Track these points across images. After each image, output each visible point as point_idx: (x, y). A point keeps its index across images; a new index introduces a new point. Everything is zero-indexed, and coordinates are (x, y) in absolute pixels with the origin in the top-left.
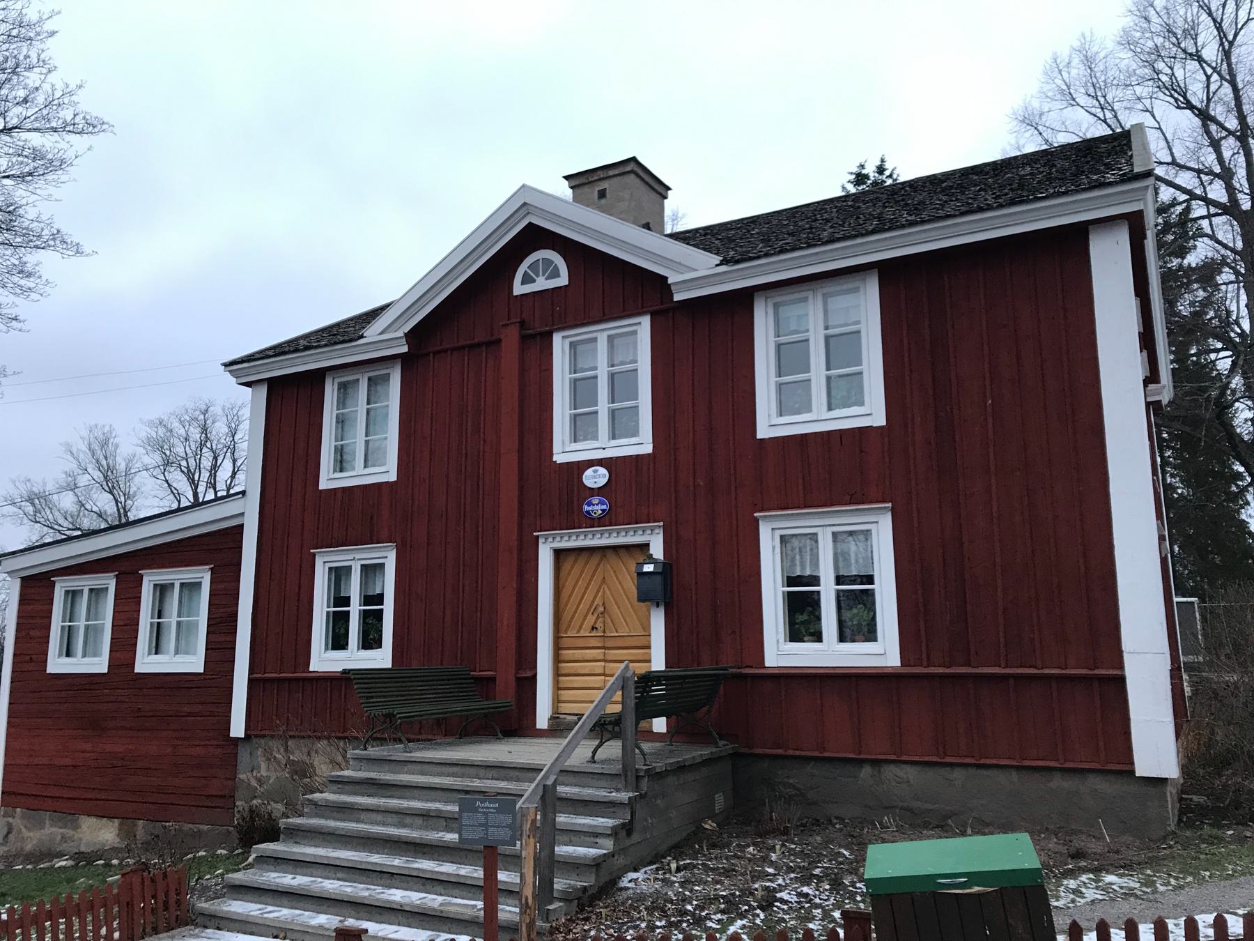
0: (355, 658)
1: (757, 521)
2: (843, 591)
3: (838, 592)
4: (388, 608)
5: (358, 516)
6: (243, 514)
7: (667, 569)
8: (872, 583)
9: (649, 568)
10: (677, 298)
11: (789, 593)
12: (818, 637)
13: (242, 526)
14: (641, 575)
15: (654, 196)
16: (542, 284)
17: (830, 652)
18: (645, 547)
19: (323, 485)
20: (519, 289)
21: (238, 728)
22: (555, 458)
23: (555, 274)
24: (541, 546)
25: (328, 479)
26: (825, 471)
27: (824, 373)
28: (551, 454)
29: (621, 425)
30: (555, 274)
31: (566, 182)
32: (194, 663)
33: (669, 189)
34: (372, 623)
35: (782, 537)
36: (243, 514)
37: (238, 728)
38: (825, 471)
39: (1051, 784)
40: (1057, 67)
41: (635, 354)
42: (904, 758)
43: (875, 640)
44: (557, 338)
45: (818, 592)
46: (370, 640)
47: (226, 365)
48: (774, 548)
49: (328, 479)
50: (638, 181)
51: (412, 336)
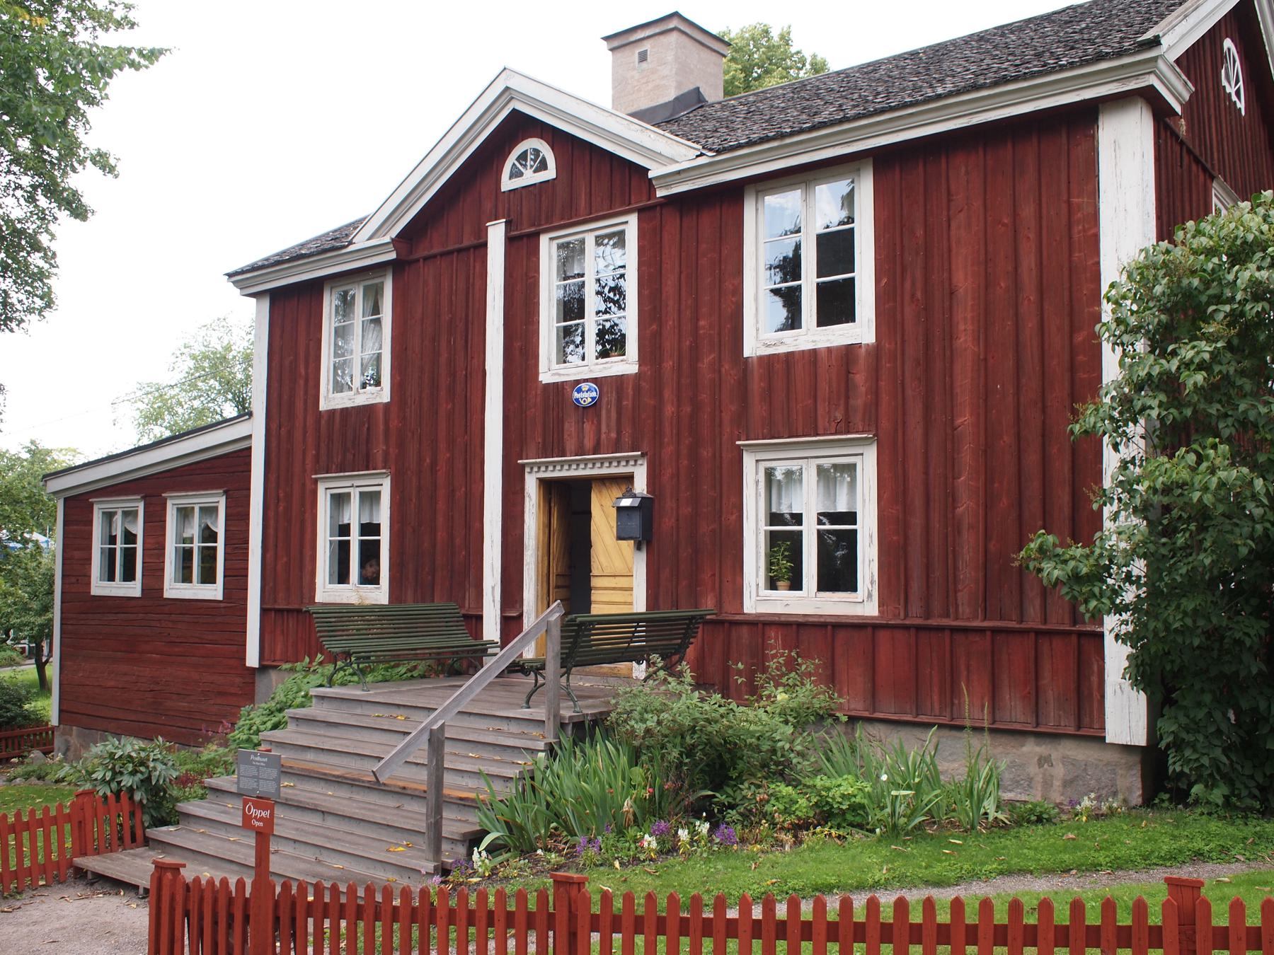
0: (352, 593)
2: (829, 532)
4: (385, 538)
6: (250, 437)
7: (646, 505)
9: (626, 502)
10: (660, 193)
11: (772, 532)
13: (250, 448)
16: (530, 177)
18: (629, 478)
19: (323, 406)
20: (507, 184)
21: (252, 659)
23: (543, 166)
24: (527, 476)
25: (330, 400)
26: (800, 400)
29: (611, 343)
30: (543, 166)
31: (605, 43)
32: (215, 592)
34: (370, 553)
36: (250, 437)
37: (252, 659)
38: (800, 400)
39: (1024, 749)
42: (877, 715)
43: (801, 589)
44: (544, 240)
45: (855, 531)
46: (129, 576)
47: (230, 275)
48: (757, 482)
49: (330, 400)
50: (683, 38)
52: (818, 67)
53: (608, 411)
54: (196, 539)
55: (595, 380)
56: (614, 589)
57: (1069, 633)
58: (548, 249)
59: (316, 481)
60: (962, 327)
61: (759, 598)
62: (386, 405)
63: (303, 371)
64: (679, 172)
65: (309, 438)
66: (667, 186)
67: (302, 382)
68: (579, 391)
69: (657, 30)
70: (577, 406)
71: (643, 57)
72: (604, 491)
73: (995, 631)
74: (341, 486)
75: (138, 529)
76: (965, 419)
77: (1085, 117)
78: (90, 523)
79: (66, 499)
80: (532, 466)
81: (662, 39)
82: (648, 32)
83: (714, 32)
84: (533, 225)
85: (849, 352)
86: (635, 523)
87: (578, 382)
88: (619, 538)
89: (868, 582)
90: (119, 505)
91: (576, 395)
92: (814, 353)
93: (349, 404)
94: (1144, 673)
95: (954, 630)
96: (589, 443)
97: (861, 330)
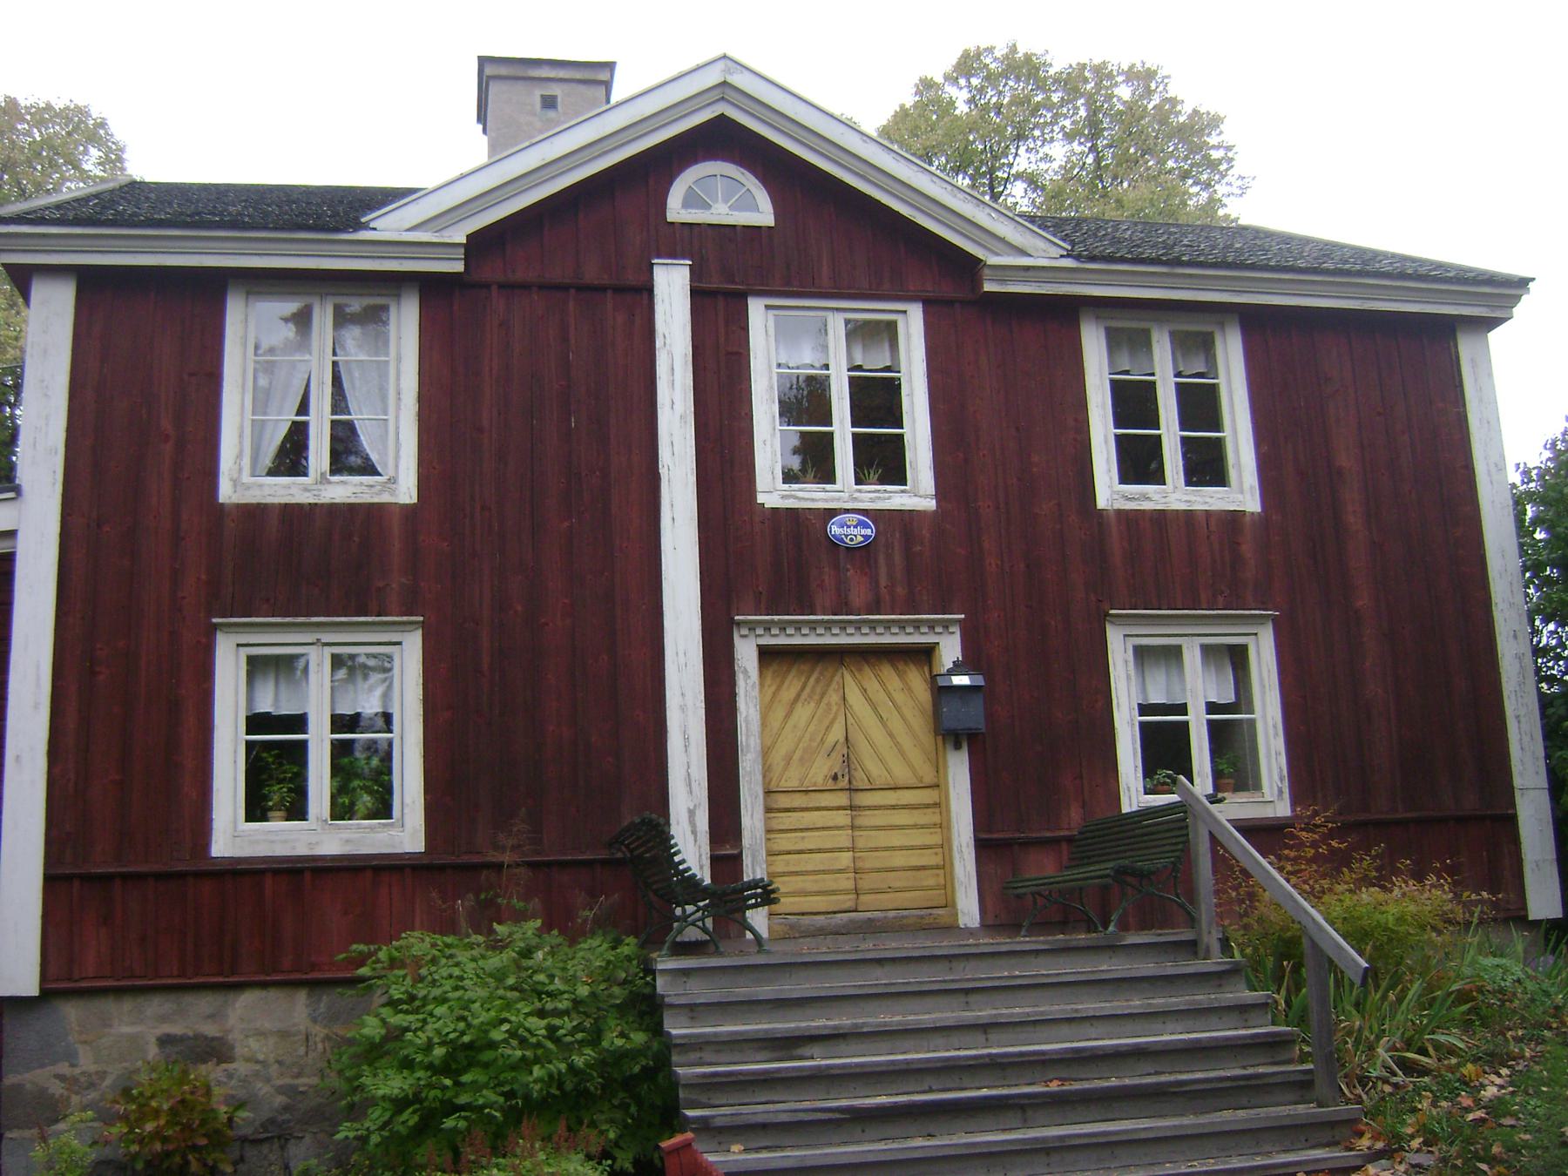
10: (988, 287)
12: (297, 811)
16: (721, 213)
17: (318, 835)
18: (926, 654)
22: (761, 499)
25: (241, 477)
26: (1178, 568)
27: (328, 417)
35: (333, 656)
40: (917, 86)
41: (1152, 367)
51: (479, 244)
56: (893, 807)
59: (215, 627)
62: (405, 508)
63: (166, 424)
64: (1027, 268)
66: (1002, 281)
67: (168, 448)
69: (578, 75)
70: (834, 546)
71: (549, 103)
74: (275, 641)
76: (1363, 601)
81: (582, 88)
82: (562, 74)
83: (837, 113)
85: (1233, 519)
87: (832, 513)
89: (1276, 777)
92: (1189, 515)
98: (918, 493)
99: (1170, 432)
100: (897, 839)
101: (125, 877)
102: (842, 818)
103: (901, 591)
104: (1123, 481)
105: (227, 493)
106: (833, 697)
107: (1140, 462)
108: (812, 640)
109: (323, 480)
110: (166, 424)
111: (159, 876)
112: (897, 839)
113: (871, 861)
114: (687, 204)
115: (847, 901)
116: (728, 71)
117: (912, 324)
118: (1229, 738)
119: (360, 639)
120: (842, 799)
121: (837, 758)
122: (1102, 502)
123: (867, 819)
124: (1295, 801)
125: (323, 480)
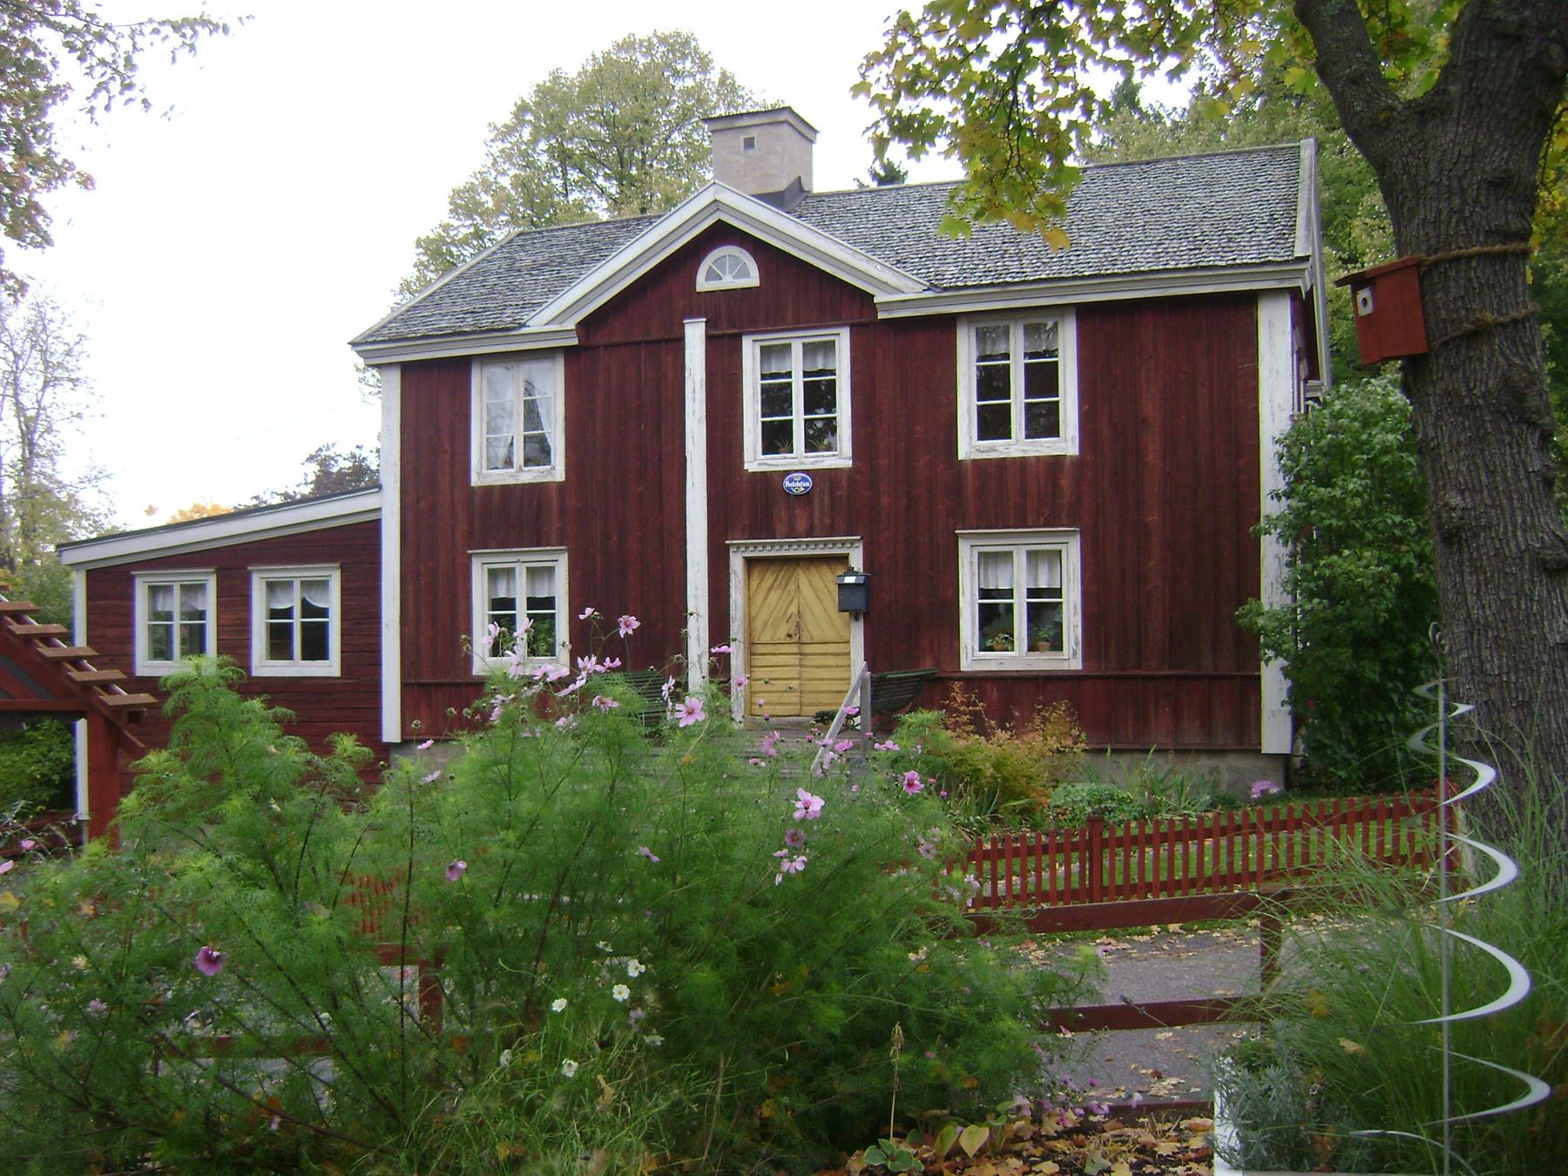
1: (956, 537)
3: (981, 605)
5: (515, 518)
8: (326, 616)
9: (850, 580)
10: (880, 316)
14: (842, 586)
15: (803, 143)
16: (729, 282)
22: (746, 466)
23: (744, 273)
25: (482, 474)
26: (1015, 498)
28: (742, 462)
30: (744, 273)
32: (330, 667)
33: (816, 132)
37: (391, 731)
38: (1015, 498)
51: (584, 325)
52: (727, 85)
53: (821, 499)
54: (297, 612)
55: (807, 472)
57: (1233, 677)
58: (750, 349)
60: (1151, 447)
61: (972, 657)
62: (560, 484)
63: (447, 446)
65: (450, 512)
67: (447, 457)
68: (791, 480)
70: (787, 495)
71: (749, 143)
72: (813, 569)
73: (1177, 678)
74: (501, 561)
75: (209, 602)
76: (1153, 518)
77: (1249, 301)
78: (131, 597)
79: (90, 573)
80: (738, 546)
82: (756, 121)
84: (734, 326)
85: (1056, 462)
86: (859, 600)
87: (788, 473)
88: (842, 610)
90: (176, 579)
91: (787, 484)
92: (1023, 461)
93: (512, 481)
94: (1300, 701)
95: (1144, 678)
96: (801, 525)
97: (1067, 443)
98: (840, 456)
99: (1018, 400)
100: (825, 673)
101: (436, 685)
102: (794, 660)
103: (827, 521)
104: (980, 438)
105: (475, 481)
106: (792, 587)
107: (993, 424)
108: (783, 553)
109: (520, 470)
110: (447, 446)
111: (450, 685)
112: (825, 673)
113: (811, 686)
114: (707, 279)
115: (795, 709)
116: (716, 192)
117: (843, 339)
118: (1043, 612)
119: (539, 558)
120: (794, 649)
121: (793, 623)
122: (962, 455)
123: (810, 661)
124: (1085, 659)
125: (520, 470)
